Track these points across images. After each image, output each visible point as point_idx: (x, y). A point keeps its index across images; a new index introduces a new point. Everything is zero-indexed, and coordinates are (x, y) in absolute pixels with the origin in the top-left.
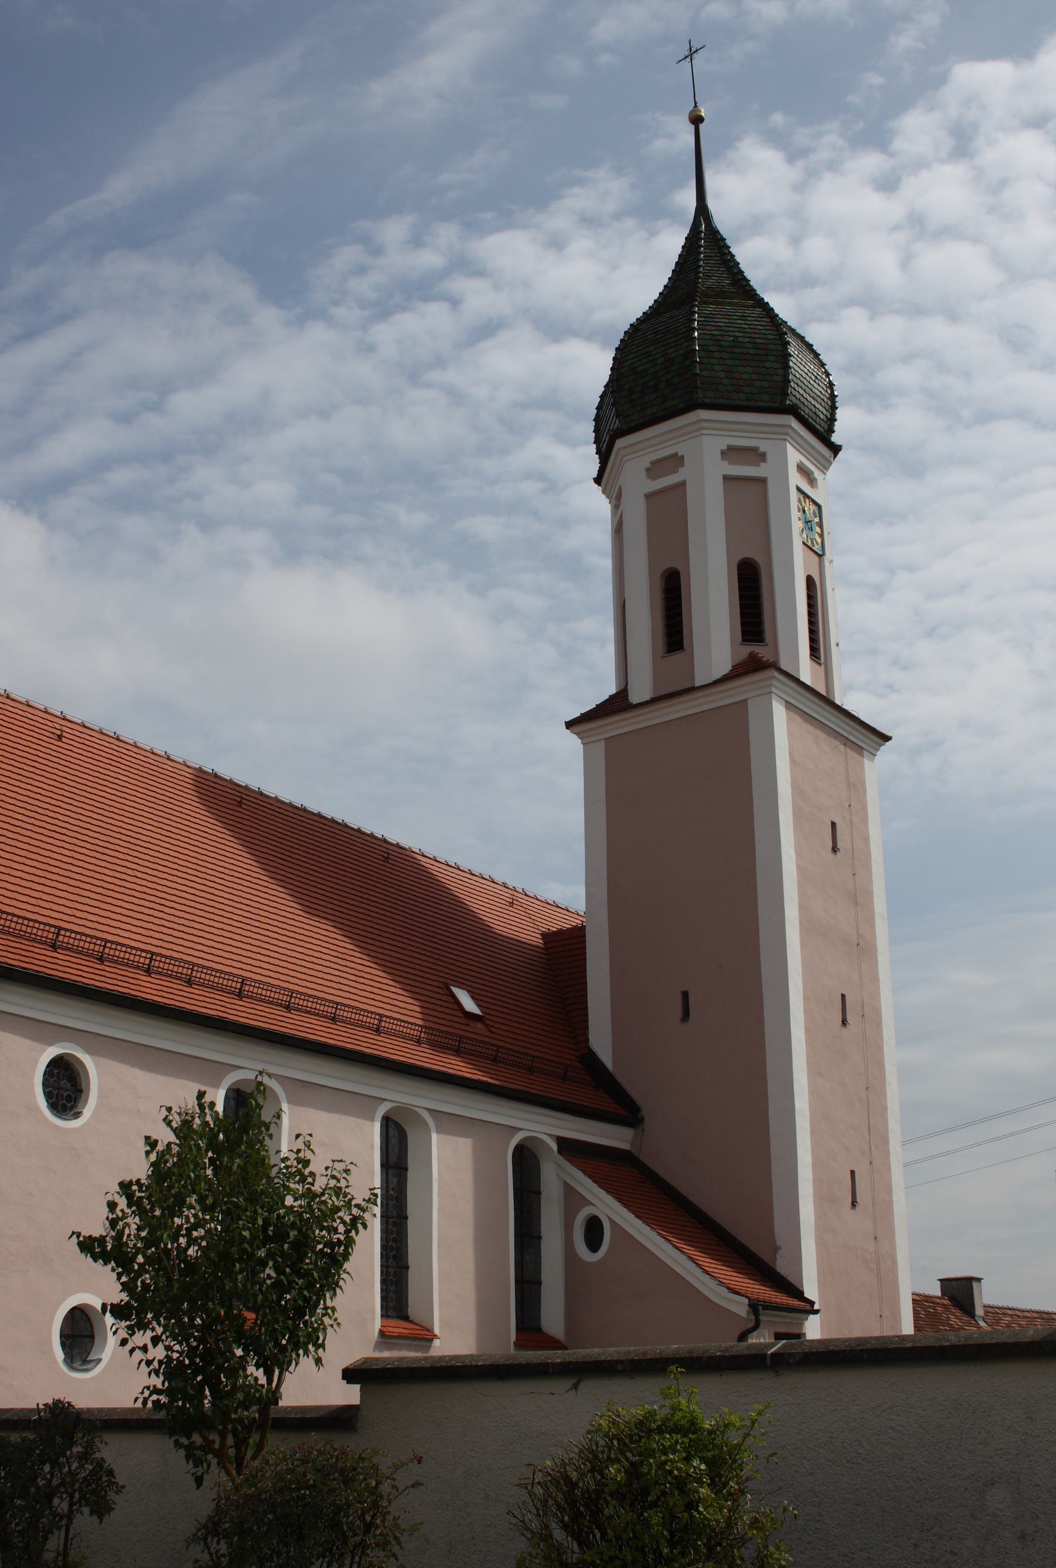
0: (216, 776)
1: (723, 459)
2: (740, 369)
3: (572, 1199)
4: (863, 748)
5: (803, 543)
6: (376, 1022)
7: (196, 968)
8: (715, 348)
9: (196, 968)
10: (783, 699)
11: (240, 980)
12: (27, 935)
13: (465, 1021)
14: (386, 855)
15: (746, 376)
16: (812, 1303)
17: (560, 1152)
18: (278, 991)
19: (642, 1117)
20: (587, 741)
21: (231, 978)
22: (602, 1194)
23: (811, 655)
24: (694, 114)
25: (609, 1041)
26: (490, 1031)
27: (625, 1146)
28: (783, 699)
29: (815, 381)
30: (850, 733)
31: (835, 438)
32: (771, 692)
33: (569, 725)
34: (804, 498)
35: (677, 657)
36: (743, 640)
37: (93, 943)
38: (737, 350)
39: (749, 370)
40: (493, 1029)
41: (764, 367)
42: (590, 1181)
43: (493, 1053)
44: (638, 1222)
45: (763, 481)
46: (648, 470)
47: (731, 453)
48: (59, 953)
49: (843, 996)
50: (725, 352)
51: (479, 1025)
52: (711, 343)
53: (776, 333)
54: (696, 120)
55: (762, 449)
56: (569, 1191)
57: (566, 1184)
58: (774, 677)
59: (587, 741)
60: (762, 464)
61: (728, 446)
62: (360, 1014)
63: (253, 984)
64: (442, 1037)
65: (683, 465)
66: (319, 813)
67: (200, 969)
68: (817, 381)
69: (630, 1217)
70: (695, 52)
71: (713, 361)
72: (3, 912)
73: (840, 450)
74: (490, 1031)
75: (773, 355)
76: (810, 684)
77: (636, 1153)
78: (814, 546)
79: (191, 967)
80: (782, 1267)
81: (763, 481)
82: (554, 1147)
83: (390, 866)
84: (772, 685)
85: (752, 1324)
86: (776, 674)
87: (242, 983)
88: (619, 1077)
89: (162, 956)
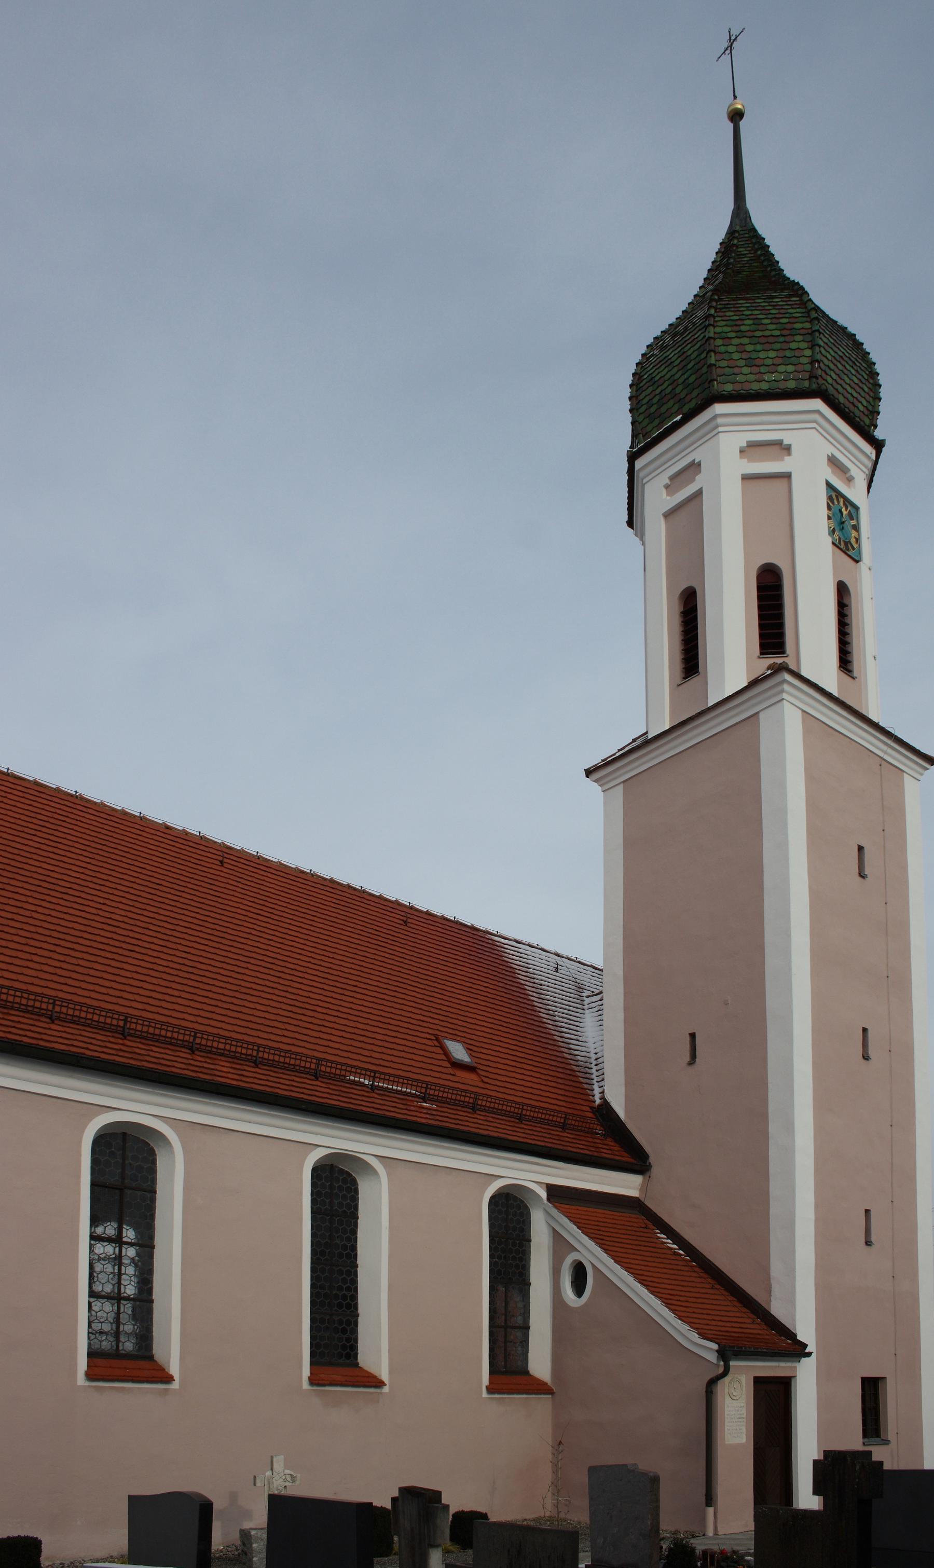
0: (168, 827)
1: (741, 458)
2: (762, 355)
3: (560, 1245)
4: (903, 771)
5: (833, 543)
6: (562, 1121)
7: (525, 1107)
8: (733, 335)
9: (261, 1049)
10: (799, 708)
11: (563, 1116)
12: (291, 1066)
13: (451, 1071)
14: (405, 919)
15: (769, 362)
16: (805, 1346)
17: (549, 1199)
18: (437, 1088)
19: (650, 1163)
20: (600, 784)
21: (513, 1105)
22: (585, 1239)
23: (840, 666)
24: (732, 108)
25: (622, 1090)
26: (482, 1081)
27: (634, 1193)
28: (799, 708)
29: (852, 367)
30: (886, 753)
31: (879, 434)
32: (783, 699)
33: (589, 773)
34: (837, 497)
35: (694, 681)
36: (761, 654)
37: (334, 1067)
38: (758, 334)
39: (772, 354)
40: (485, 1080)
41: (790, 349)
42: (575, 1227)
43: (471, 1101)
44: (617, 1268)
45: (788, 476)
46: (667, 487)
47: (752, 449)
48: (260, 1068)
49: (865, 1030)
50: (745, 336)
51: (473, 1076)
52: (729, 329)
53: (804, 310)
54: (736, 116)
55: (786, 442)
56: (557, 1237)
57: (555, 1231)
58: (785, 681)
59: (600, 784)
60: (787, 458)
61: (747, 442)
62: (487, 1101)
63: (497, 1101)
64: (542, 1113)
65: (700, 472)
66: (331, 878)
67: (485, 1099)
68: (855, 367)
69: (610, 1262)
70: (734, 40)
71: (732, 349)
72: (2, 986)
73: (883, 446)
74: (482, 1081)
75: (800, 335)
76: (837, 695)
77: (642, 1200)
78: (849, 550)
79: (256, 1048)
80: (777, 1310)
81: (788, 476)
82: (543, 1194)
83: (409, 929)
84: (783, 691)
85: (721, 1370)
86: (787, 677)
87: (426, 1088)
88: (630, 1126)
89: (328, 1061)
